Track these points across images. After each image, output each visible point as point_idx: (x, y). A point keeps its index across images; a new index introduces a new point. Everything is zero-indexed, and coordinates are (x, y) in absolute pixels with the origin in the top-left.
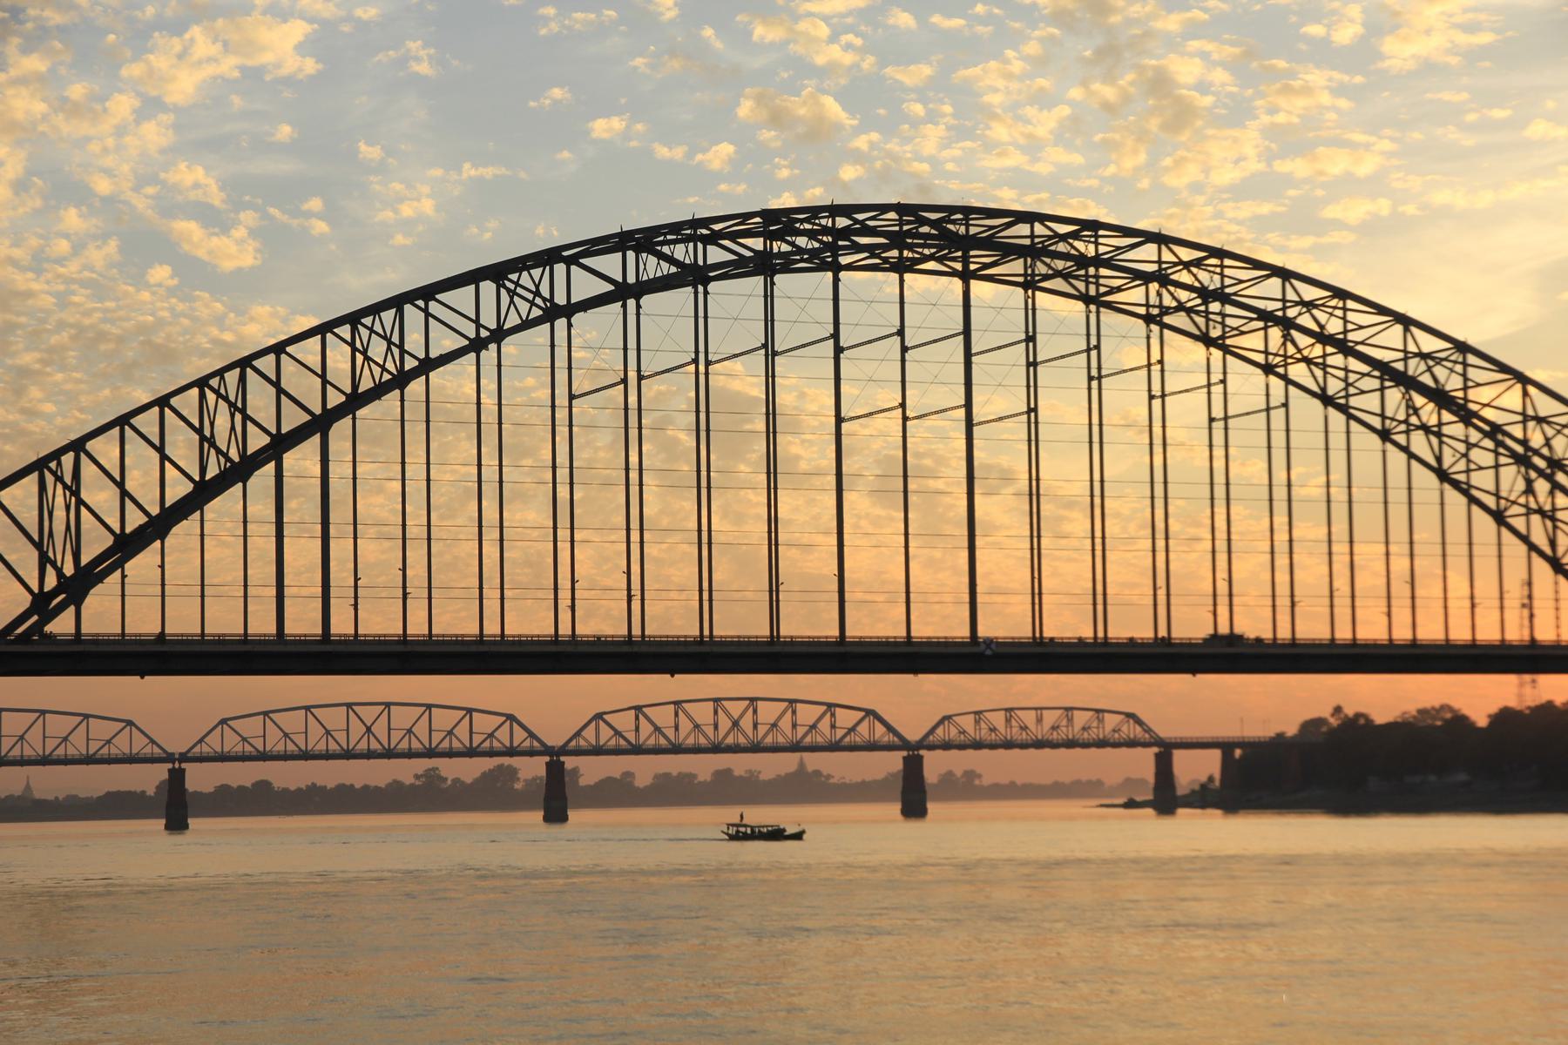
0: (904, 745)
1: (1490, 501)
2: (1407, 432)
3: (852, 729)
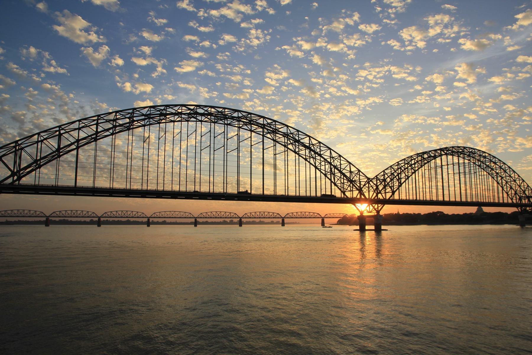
0: (282, 218)
1: (324, 172)
2: (310, 159)
3: (85, 214)
